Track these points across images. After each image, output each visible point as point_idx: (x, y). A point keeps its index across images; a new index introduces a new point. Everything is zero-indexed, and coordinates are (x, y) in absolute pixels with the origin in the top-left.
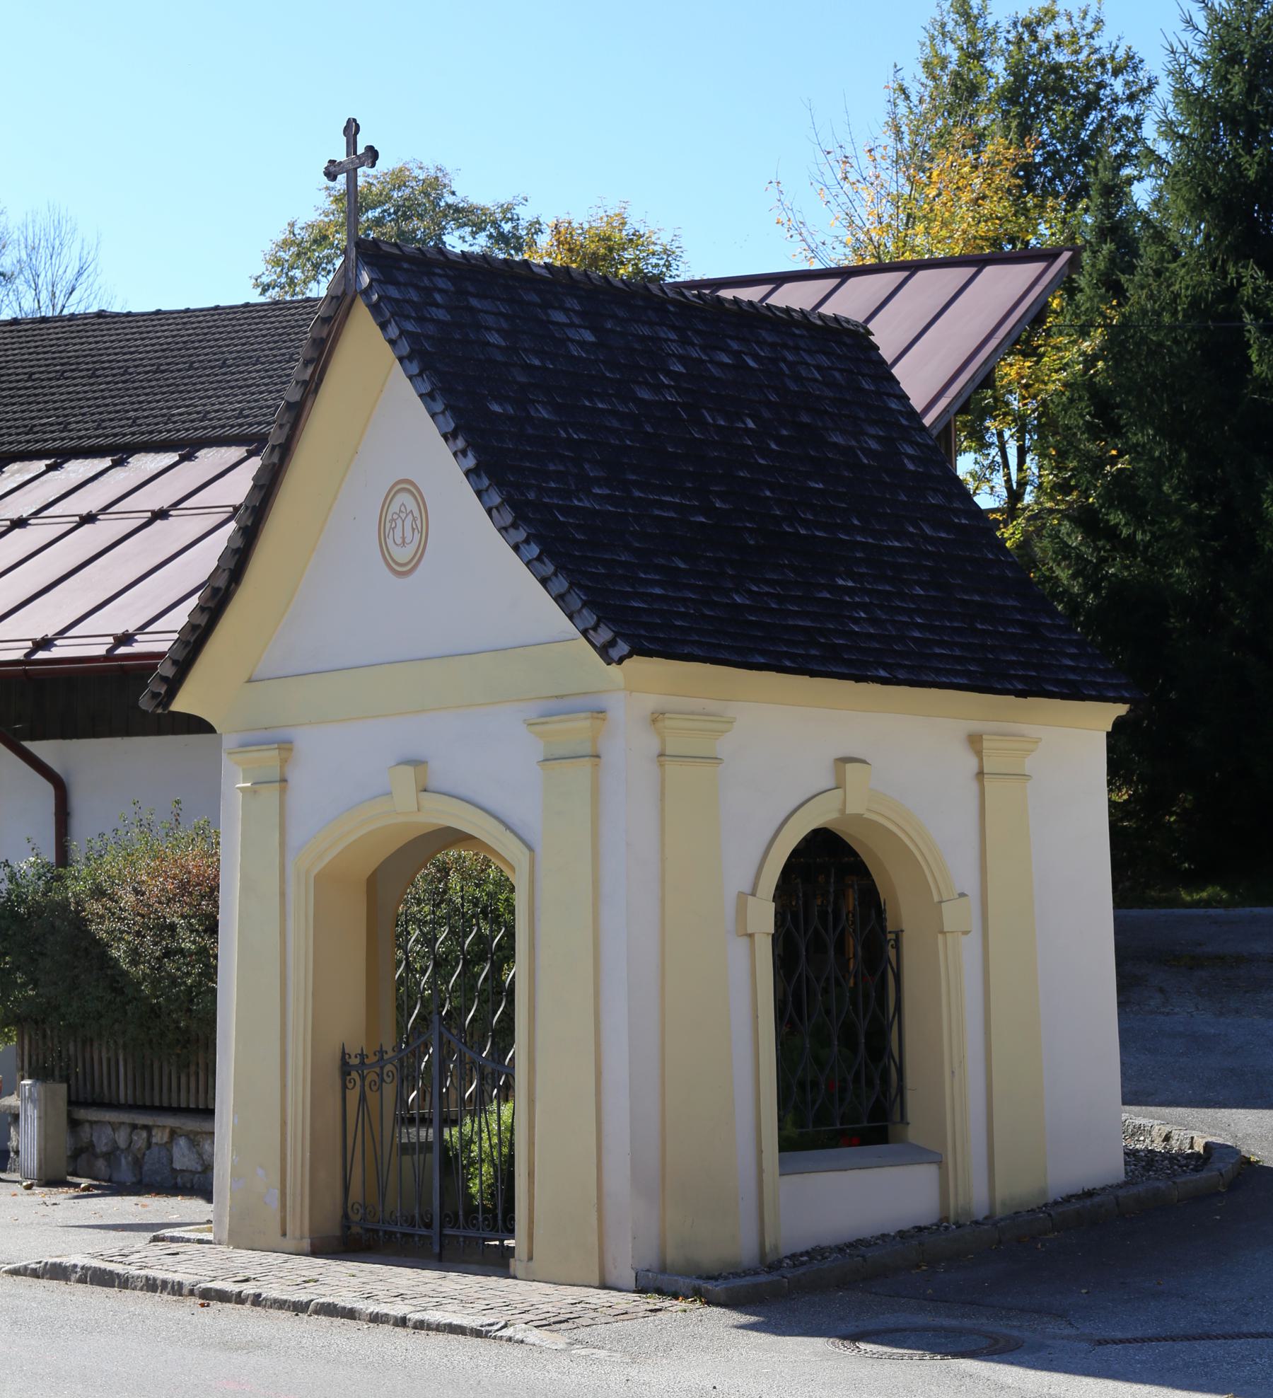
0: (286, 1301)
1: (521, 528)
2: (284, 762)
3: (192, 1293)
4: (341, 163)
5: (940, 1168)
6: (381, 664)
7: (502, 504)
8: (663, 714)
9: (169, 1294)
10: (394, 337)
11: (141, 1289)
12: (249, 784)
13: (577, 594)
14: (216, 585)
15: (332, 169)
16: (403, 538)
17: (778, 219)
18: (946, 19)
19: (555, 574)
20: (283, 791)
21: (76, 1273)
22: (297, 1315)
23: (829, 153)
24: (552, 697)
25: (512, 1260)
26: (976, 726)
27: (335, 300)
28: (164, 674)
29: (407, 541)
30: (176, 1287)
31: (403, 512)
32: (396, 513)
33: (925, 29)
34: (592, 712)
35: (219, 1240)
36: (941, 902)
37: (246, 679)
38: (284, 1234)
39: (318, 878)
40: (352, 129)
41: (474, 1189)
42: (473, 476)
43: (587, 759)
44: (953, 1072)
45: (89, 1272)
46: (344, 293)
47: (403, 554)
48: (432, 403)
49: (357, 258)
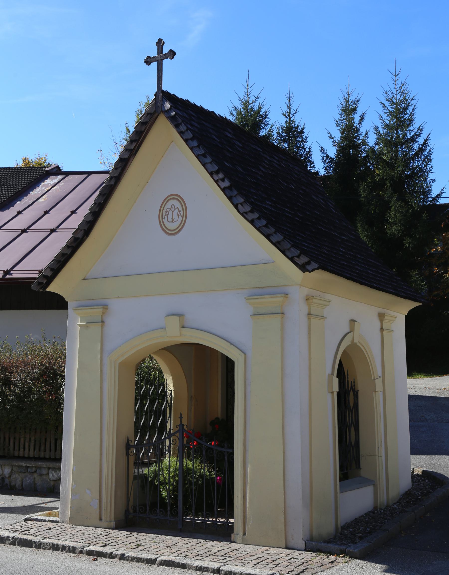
0: (141, 558)
1: (255, 212)
2: (103, 313)
3: (81, 552)
4: (154, 57)
5: (374, 487)
6: (192, 270)
7: (245, 202)
8: (313, 296)
9: (67, 552)
10: (183, 130)
11: (49, 549)
12: (85, 323)
13: (287, 241)
14: (77, 237)
15: (149, 60)
16: (173, 219)
17: (100, 162)
18: (142, 110)
19: (275, 233)
20: (102, 326)
21: (9, 540)
22: (151, 566)
23: (117, 143)
24: (257, 288)
25: (232, 535)
26: (383, 311)
27: (149, 115)
28: (45, 275)
29: (175, 220)
30: (71, 549)
31: (173, 208)
32: (169, 208)
33: (136, 112)
34: (284, 294)
35: (63, 521)
36: (375, 379)
37: (82, 279)
38: (101, 519)
39: (120, 364)
40: (160, 44)
41: (164, 494)
42: (227, 191)
43: (280, 314)
44: (379, 448)
45: (17, 540)
46: (155, 112)
47: (172, 226)
48: (205, 159)
49: (162, 97)
